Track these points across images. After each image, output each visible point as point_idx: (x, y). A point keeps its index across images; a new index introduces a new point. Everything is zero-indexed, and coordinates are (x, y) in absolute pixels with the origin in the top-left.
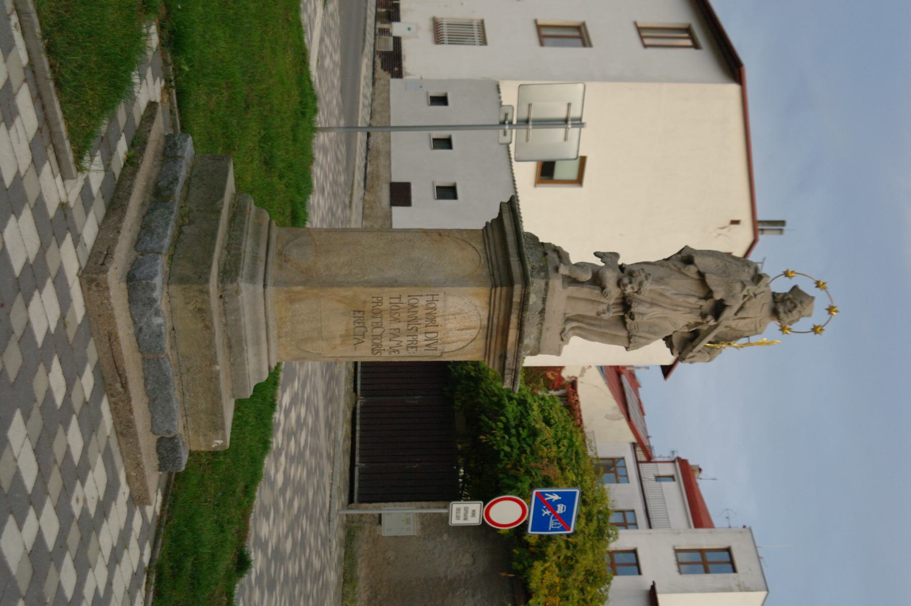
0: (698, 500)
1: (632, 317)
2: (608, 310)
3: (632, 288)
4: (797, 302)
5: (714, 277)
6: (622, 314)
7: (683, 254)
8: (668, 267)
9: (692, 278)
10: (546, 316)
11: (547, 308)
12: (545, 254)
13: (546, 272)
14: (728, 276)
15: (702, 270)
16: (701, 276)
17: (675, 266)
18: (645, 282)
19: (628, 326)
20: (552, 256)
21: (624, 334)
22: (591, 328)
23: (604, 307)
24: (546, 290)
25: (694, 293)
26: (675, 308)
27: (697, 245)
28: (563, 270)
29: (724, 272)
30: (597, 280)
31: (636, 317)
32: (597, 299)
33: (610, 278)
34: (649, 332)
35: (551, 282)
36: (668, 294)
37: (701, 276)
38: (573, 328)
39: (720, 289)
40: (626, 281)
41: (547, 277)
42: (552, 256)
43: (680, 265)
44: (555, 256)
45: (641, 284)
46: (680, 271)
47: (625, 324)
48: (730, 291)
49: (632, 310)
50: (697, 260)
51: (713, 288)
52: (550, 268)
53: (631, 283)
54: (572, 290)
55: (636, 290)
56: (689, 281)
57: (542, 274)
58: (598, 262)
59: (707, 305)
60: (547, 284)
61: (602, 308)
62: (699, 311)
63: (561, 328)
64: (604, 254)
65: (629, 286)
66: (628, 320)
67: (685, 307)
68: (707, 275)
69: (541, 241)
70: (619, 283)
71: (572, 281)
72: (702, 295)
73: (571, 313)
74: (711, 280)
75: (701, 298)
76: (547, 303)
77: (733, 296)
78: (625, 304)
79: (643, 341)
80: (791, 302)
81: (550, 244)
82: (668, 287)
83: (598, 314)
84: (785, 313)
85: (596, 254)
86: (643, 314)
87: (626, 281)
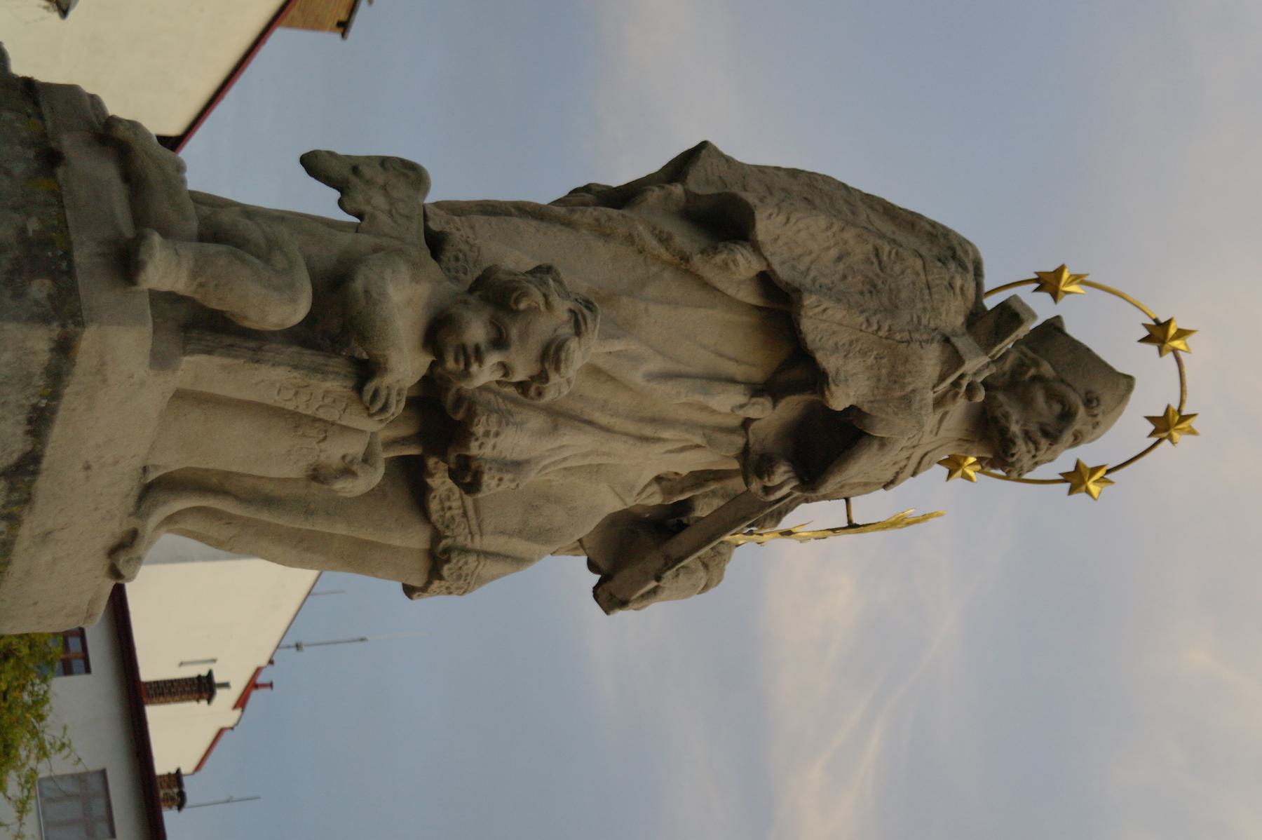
0: (222, 553)
1: (468, 477)
2: (367, 459)
3: (505, 368)
4: (1076, 399)
5: (837, 313)
6: (413, 451)
7: (699, 182)
8: (630, 239)
9: (731, 303)
10: (43, 484)
11: (51, 455)
12: (51, 159)
13: (62, 273)
14: (892, 309)
15: (783, 273)
16: (778, 305)
17: (665, 240)
18: (573, 344)
19: (434, 506)
20: (91, 170)
21: (415, 539)
22: (265, 516)
23: (356, 448)
24: (57, 375)
25: (731, 368)
26: (648, 431)
27: (752, 144)
28: (165, 270)
29: (873, 289)
30: (336, 330)
31: (489, 480)
32: (332, 415)
33: (402, 300)
34: (519, 533)
35: (88, 340)
36: (636, 377)
37: (778, 305)
38: (170, 519)
39: (855, 366)
40: (476, 331)
41: (66, 314)
42: (91, 170)
43: (684, 238)
44: (107, 171)
45: (552, 354)
46: (682, 265)
47: (419, 496)
48: (895, 378)
49: (474, 449)
50: (766, 226)
51: (829, 362)
52: (84, 254)
53: (499, 342)
54: (204, 370)
55: (520, 375)
56: (719, 314)
57: (39, 289)
58: (321, 201)
59: (770, 417)
60: (64, 348)
61: (335, 451)
62: (739, 441)
63: (115, 529)
64: (355, 166)
65: (493, 359)
66: (440, 482)
67: (690, 426)
68: (809, 300)
69: (19, 68)
70: (438, 331)
71: (201, 325)
72: (757, 375)
73: (171, 461)
74: (822, 323)
75: (758, 390)
76: (57, 433)
77: (907, 401)
78: (441, 424)
79: (490, 567)
80: (1051, 396)
81: (70, 93)
82: (633, 346)
83: (317, 475)
84: (1028, 436)
85: (313, 164)
86: (516, 466)
87: (476, 331)
